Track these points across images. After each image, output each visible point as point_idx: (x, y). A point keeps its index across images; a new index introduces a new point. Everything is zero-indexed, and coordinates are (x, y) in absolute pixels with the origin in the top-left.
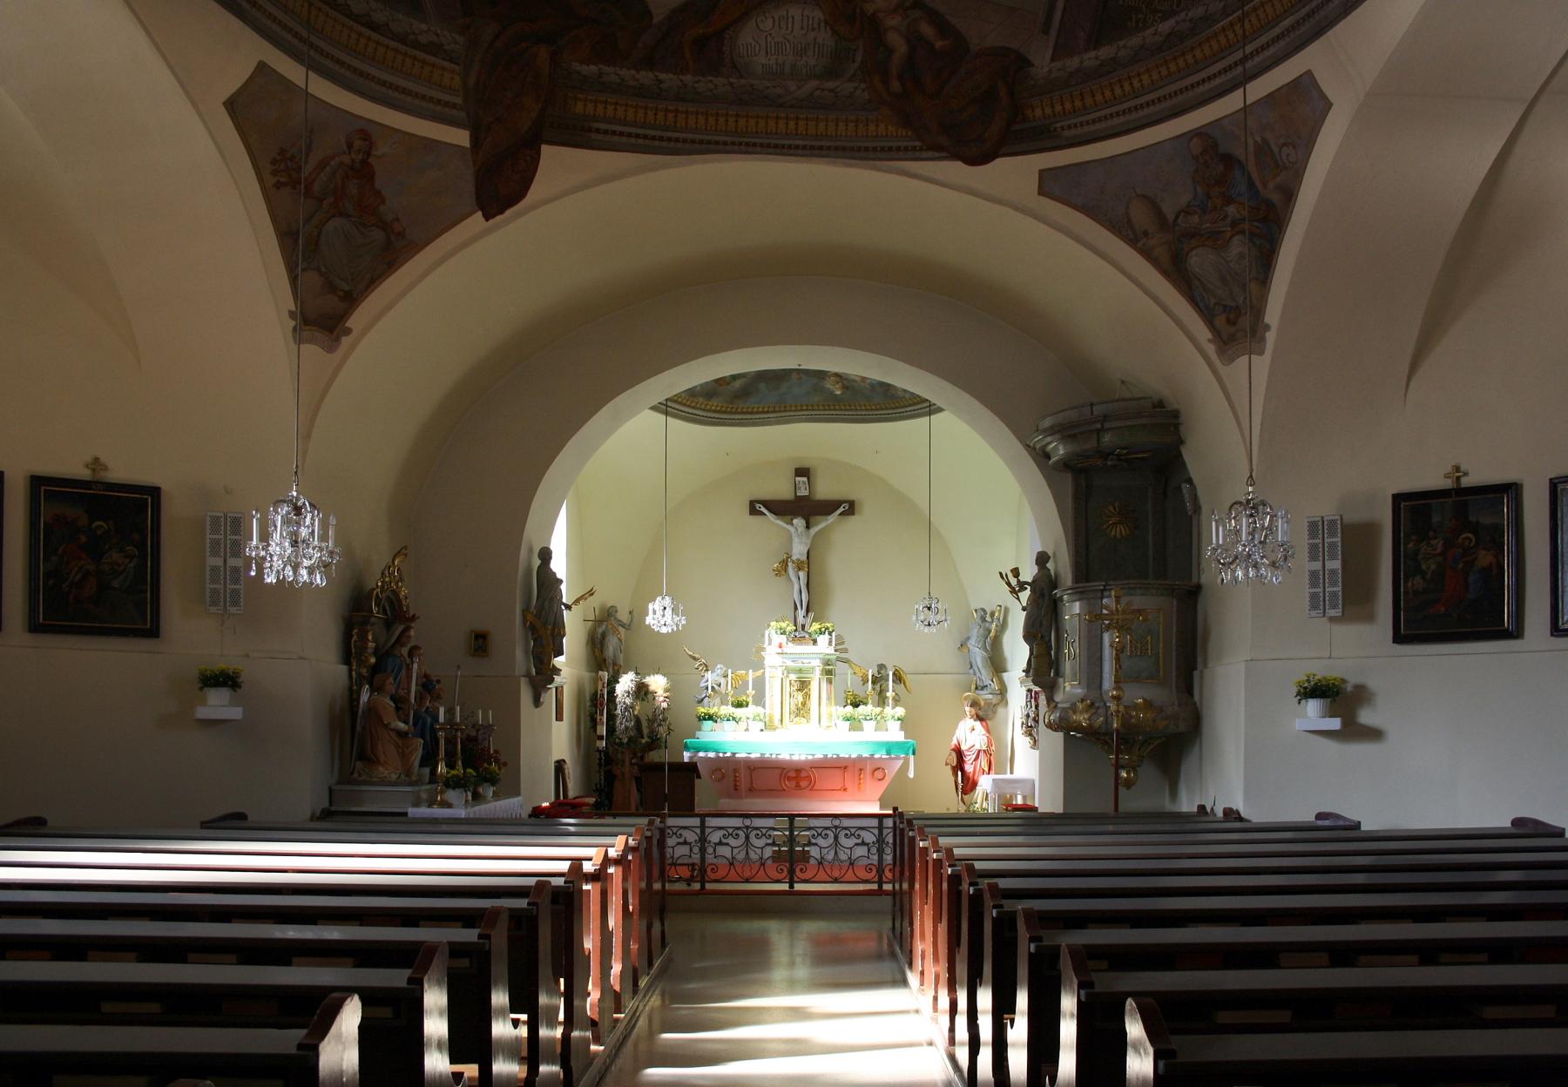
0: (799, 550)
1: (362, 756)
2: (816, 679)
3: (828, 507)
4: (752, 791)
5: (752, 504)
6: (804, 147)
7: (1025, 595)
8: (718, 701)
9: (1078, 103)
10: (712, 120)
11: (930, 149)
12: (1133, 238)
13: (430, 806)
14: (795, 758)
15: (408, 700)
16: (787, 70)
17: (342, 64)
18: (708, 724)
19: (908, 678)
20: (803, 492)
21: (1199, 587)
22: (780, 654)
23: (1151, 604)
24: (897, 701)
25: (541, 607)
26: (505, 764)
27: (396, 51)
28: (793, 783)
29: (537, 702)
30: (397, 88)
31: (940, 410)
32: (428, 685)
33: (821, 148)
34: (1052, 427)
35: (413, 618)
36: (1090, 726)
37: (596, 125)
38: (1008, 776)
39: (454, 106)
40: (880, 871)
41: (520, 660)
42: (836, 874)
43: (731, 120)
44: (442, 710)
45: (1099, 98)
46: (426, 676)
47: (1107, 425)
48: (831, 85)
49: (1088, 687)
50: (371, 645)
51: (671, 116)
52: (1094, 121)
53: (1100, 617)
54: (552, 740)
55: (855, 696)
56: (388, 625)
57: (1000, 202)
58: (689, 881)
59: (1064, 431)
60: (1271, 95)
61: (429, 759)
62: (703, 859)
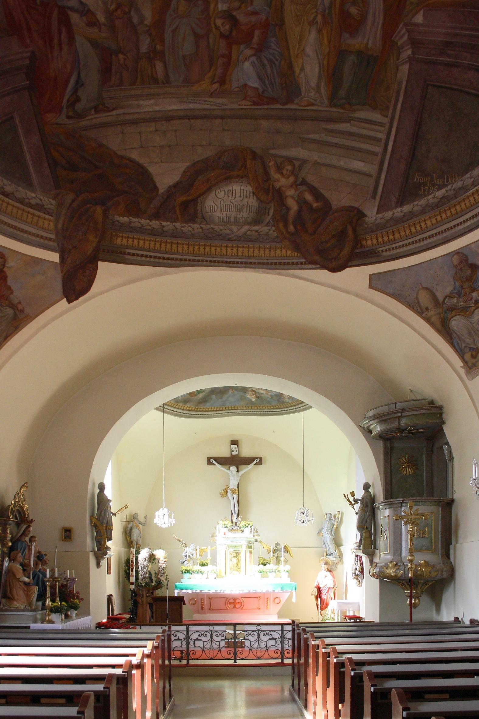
0: (233, 484)
1: (5, 596)
2: (244, 551)
3: (248, 461)
4: (211, 610)
5: (208, 459)
6: (242, 263)
7: (357, 506)
8: (192, 563)
9: (391, 237)
10: (191, 248)
11: (310, 263)
12: (421, 312)
13: (42, 623)
14: (233, 593)
15: (30, 565)
16: (232, 220)
18: (187, 575)
19: (291, 550)
20: (235, 453)
21: (453, 501)
22: (224, 539)
23: (428, 510)
24: (286, 562)
25: (100, 514)
26: (82, 599)
27: (18, 208)
28: (232, 606)
29: (98, 565)
31: (311, 407)
32: (40, 557)
33: (251, 263)
34: (374, 416)
35: (32, 521)
36: (396, 575)
38: (344, 601)
39: (50, 239)
40: (282, 653)
41: (89, 543)
42: (259, 655)
43: (202, 248)
44: (48, 571)
45: (403, 234)
46: (39, 552)
47: (404, 414)
48: (256, 228)
49: (394, 555)
50: (9, 536)
51: (169, 245)
52: (400, 247)
53: (401, 518)
54: (104, 585)
55: (264, 560)
56: (18, 525)
57: (348, 292)
58: (180, 659)
59: (381, 418)
61: (41, 597)
62: (188, 648)
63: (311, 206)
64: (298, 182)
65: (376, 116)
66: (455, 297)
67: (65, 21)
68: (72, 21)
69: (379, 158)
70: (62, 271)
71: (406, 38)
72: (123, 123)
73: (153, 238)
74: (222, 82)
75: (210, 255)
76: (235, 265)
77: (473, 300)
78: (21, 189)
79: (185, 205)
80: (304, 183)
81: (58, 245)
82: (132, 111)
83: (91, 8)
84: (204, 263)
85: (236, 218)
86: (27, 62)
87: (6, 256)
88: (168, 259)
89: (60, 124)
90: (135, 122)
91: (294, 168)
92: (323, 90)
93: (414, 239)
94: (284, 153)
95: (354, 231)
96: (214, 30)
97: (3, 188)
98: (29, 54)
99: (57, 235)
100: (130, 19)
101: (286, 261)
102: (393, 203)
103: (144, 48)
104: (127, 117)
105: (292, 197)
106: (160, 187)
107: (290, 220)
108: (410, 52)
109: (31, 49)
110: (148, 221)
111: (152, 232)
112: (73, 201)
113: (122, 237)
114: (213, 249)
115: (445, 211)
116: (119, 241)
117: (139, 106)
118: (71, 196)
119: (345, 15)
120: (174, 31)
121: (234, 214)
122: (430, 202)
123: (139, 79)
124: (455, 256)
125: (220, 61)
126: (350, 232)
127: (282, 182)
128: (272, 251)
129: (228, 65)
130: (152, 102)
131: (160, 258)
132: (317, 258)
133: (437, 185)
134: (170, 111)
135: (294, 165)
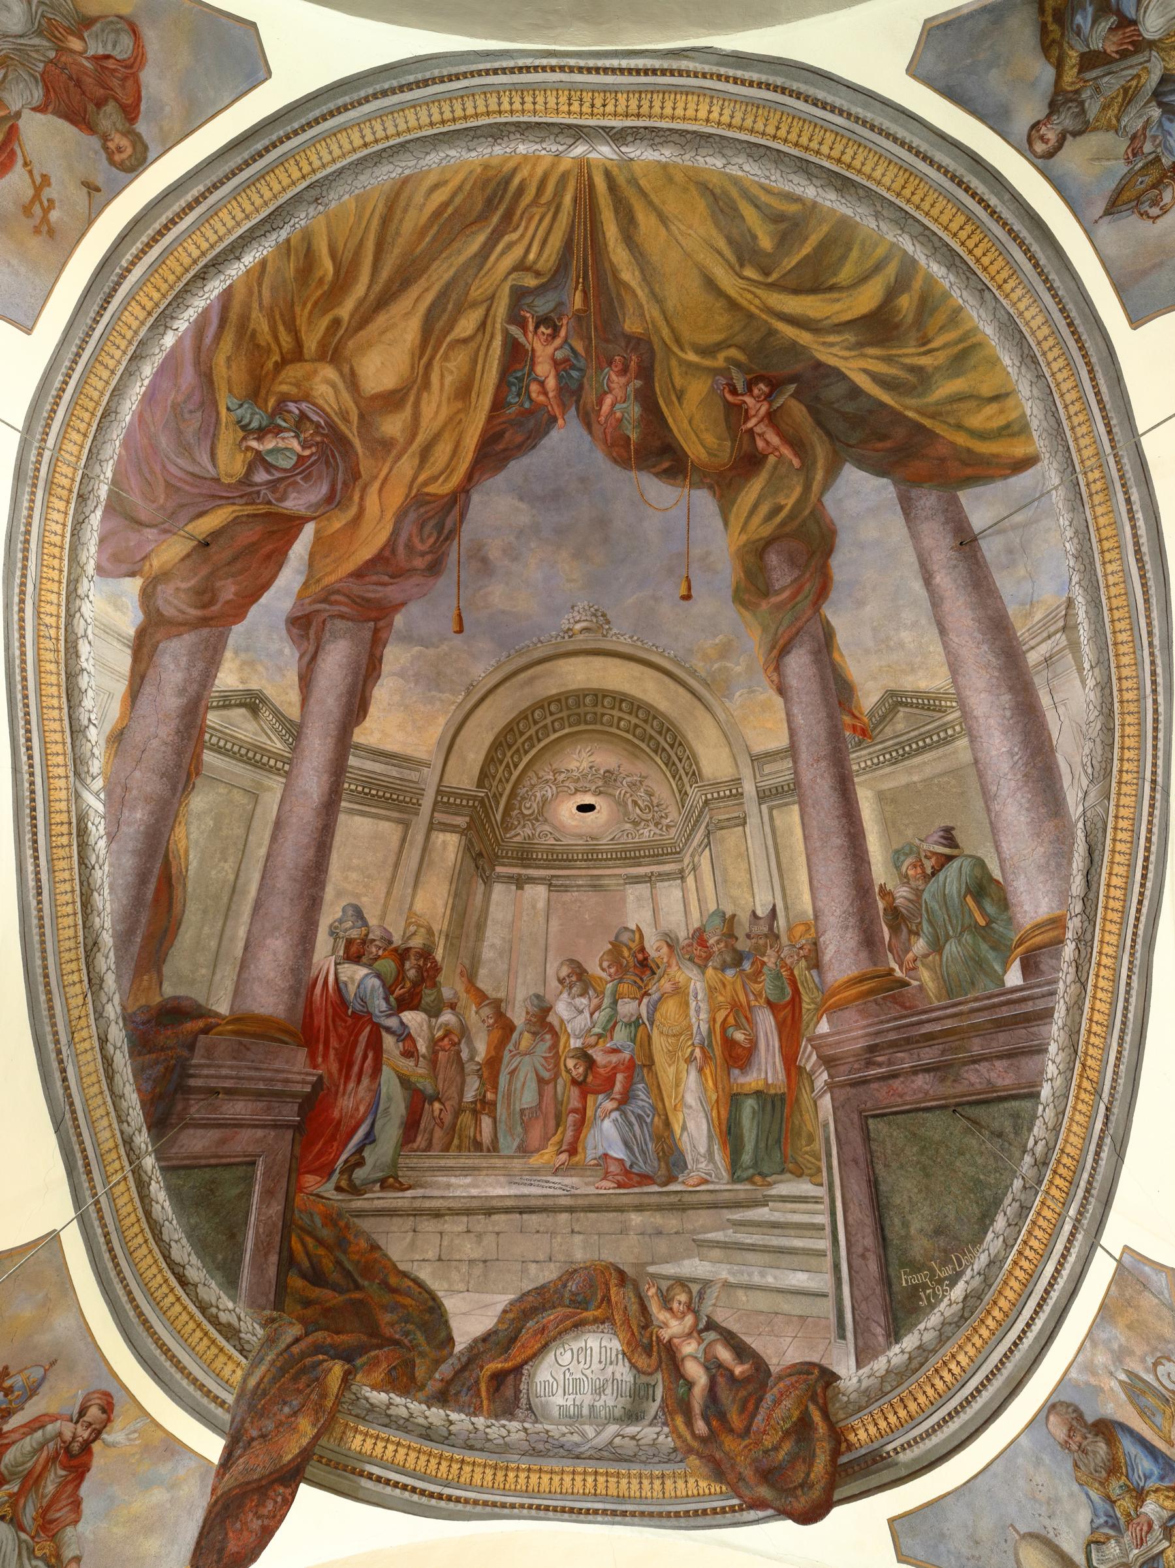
11: (757, 1504)
16: (585, 1411)
17: (132, 1300)
27: (192, 1317)
33: (624, 1513)
39: (222, 1404)
43: (523, 1475)
48: (631, 1430)
54: (186, 1053)
60: (1103, 1306)
63: (732, 1372)
64: (701, 1326)
65: (805, 1188)
66: (1108, 1538)
67: (375, 1045)
69: (829, 1258)
70: (214, 1490)
71: (814, 1057)
72: (417, 1213)
73: (427, 1446)
74: (573, 1151)
75: (538, 1493)
76: (590, 1517)
77: (1156, 1527)
78: (213, 1285)
79: (498, 1379)
80: (711, 1325)
82: (436, 1193)
85: (592, 1407)
86: (308, 1089)
87: (117, 1410)
90: (437, 1214)
91: (691, 1299)
92: (717, 1157)
94: (670, 1269)
99: (237, 1400)
100: (458, 1052)
102: (881, 1339)
103: (469, 1096)
104: (427, 1204)
106: (457, 1339)
107: (697, 1408)
108: (825, 1076)
110: (424, 1407)
111: (427, 1433)
112: (297, 1340)
113: (366, 1434)
115: (982, 1321)
116: (356, 1443)
117: (448, 1186)
118: (296, 1330)
120: (512, 1073)
121: (588, 1399)
122: (947, 1314)
123: (456, 1142)
124: (1052, 1418)
125: (571, 1118)
126: (817, 1417)
127: (673, 1327)
129: (580, 1125)
130: (468, 1180)
132: (764, 1492)
133: (946, 1278)
135: (690, 1292)
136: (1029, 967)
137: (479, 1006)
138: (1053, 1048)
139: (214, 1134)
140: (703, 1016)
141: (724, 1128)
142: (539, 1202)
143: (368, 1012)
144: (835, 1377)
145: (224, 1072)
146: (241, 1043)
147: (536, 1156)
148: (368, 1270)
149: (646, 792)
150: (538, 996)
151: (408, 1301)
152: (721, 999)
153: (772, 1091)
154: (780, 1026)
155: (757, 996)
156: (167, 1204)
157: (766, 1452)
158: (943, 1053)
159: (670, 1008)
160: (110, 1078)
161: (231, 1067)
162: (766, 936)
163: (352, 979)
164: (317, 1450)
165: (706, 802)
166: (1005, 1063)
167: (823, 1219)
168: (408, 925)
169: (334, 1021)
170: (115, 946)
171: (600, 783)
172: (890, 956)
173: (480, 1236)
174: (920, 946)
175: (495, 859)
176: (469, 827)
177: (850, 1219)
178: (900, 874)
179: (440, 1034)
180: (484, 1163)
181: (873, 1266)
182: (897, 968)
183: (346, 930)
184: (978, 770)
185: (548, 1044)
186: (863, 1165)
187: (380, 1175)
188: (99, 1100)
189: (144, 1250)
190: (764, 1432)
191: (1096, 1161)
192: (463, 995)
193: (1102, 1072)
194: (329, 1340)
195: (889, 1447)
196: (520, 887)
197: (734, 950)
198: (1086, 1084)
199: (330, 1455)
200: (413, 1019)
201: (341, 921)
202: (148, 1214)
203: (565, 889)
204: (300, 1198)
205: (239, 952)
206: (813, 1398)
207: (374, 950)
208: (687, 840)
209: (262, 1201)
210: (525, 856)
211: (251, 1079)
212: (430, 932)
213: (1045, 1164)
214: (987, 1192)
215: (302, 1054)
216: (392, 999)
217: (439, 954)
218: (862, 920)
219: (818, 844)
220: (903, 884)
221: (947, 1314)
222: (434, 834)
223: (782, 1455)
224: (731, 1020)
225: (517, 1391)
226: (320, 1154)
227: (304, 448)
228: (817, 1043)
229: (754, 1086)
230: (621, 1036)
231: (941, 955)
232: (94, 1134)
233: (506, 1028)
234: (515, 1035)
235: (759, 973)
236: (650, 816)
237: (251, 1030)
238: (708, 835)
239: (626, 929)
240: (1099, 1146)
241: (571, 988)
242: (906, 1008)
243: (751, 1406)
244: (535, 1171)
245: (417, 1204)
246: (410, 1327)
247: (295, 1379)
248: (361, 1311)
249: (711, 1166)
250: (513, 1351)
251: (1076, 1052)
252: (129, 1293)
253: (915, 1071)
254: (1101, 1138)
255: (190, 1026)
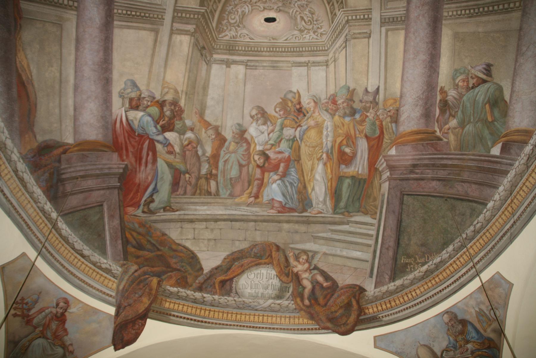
9: (388, 305)
10: (225, 315)
11: (324, 328)
16: (260, 295)
17: (64, 267)
27: (90, 268)
30: (87, 283)
33: (274, 329)
37: (173, 313)
39: (111, 296)
48: (279, 302)
52: (396, 313)
54: (57, 164)
64: (311, 268)
65: (367, 219)
66: (451, 350)
67: (152, 148)
68: (157, 149)
69: (372, 249)
70: (115, 323)
71: (385, 165)
72: (182, 221)
73: (195, 305)
74: (257, 197)
75: (240, 321)
78: (96, 255)
79: (223, 283)
81: (116, 301)
83: (171, 142)
84: (235, 327)
85: (262, 294)
86: (121, 171)
88: (206, 322)
89: (137, 216)
90: (192, 221)
91: (308, 258)
93: (408, 306)
95: (358, 302)
96: (253, 162)
97: (82, 251)
98: (124, 166)
100: (197, 151)
101: (303, 327)
103: (204, 171)
104: (186, 217)
105: (307, 279)
108: (388, 174)
109: (126, 163)
110: (193, 292)
111: (195, 301)
112: (136, 271)
114: (243, 317)
115: (430, 281)
116: (167, 305)
118: (135, 267)
119: (342, 154)
120: (225, 161)
121: (261, 291)
122: (416, 275)
123: (198, 191)
124: (445, 315)
125: (256, 183)
126: (354, 303)
127: (299, 267)
128: (291, 319)
130: (205, 208)
131: (198, 321)
132: (329, 325)
133: (420, 263)
134: (217, 215)
135: (308, 256)
136: (505, 149)
137: (206, 129)
138: (501, 188)
139: (81, 196)
140: (330, 139)
141: (333, 190)
142: (240, 217)
143: (146, 133)
144: (365, 290)
145: (78, 169)
146: (83, 154)
147: (239, 198)
148: (162, 243)
149: (310, 12)
150: (239, 125)
151: (182, 255)
152: (340, 131)
153: (360, 177)
154: (370, 149)
155: (361, 132)
156: (67, 229)
157: (332, 312)
158: (449, 174)
159: (312, 133)
160: (25, 187)
161: (81, 166)
162: (371, 102)
163: (136, 119)
164: (152, 308)
165: (347, 22)
166: (477, 186)
167: (374, 233)
168: (163, 88)
169: (129, 139)
170: (5, 126)
171: (280, 4)
172: (436, 124)
173: (212, 230)
174: (453, 123)
175: (212, 50)
176: (195, 32)
177: (385, 234)
178: (454, 83)
179: (186, 143)
180: (212, 201)
181: (391, 253)
182: (438, 130)
183: (128, 94)
184: (520, 36)
185: (245, 148)
186: (397, 214)
187: (162, 206)
188: (23, 197)
189: (63, 248)
190: (332, 306)
191: (500, 239)
192: (198, 124)
193: (519, 207)
194: (149, 270)
195: (380, 315)
196: (228, 66)
197: (352, 108)
198: (510, 209)
199: (157, 310)
200: (171, 136)
201: (124, 89)
202: (60, 235)
203: (255, 68)
204: (126, 217)
205: (71, 112)
206: (354, 297)
207: (145, 102)
208: (332, 43)
209: (109, 220)
210: (231, 49)
211: (92, 170)
212: (176, 91)
213: (479, 232)
214: (449, 235)
215: (115, 156)
216: (158, 127)
217: (182, 103)
218: (426, 103)
219: (412, 56)
220: (455, 89)
221: (416, 275)
222: (174, 36)
223: (338, 314)
224: (345, 142)
225: (231, 287)
226: (132, 199)
227: (140, 227)
228: (387, 159)
229: (351, 174)
230: (284, 146)
231: (463, 129)
232: (26, 212)
233: (221, 140)
234: (227, 144)
235: (363, 121)
236: (311, 27)
237: (86, 148)
238: (346, 41)
239: (291, 91)
240: (504, 234)
241: (257, 121)
242: (437, 150)
243: (328, 296)
244: (238, 204)
245: (182, 217)
246: (183, 264)
247: (138, 284)
248: (161, 258)
249: (324, 206)
250: (229, 273)
251: (511, 194)
252: (62, 265)
253: (433, 179)
254: (506, 232)
255: (56, 152)
